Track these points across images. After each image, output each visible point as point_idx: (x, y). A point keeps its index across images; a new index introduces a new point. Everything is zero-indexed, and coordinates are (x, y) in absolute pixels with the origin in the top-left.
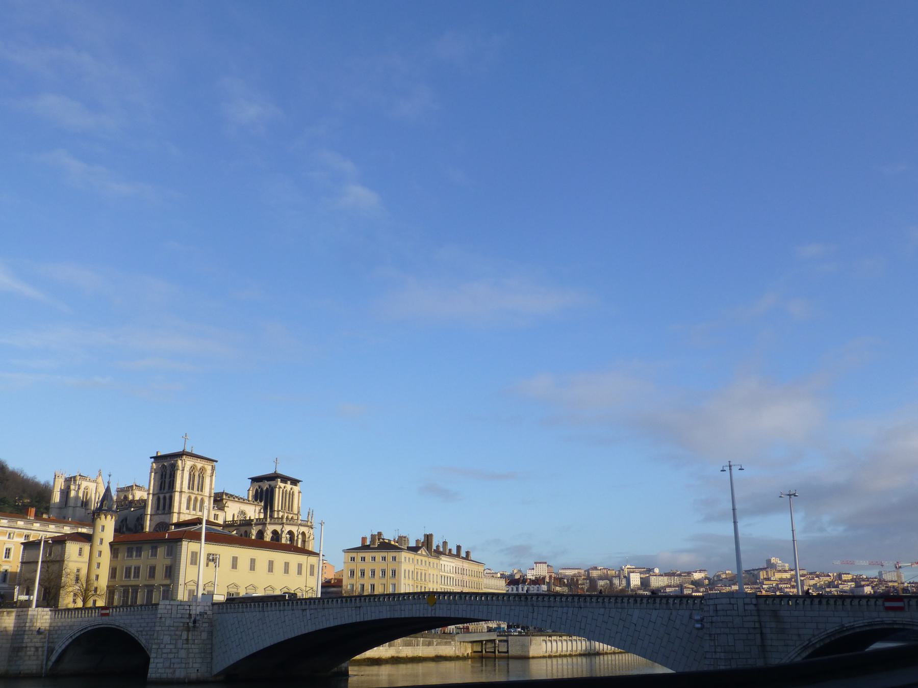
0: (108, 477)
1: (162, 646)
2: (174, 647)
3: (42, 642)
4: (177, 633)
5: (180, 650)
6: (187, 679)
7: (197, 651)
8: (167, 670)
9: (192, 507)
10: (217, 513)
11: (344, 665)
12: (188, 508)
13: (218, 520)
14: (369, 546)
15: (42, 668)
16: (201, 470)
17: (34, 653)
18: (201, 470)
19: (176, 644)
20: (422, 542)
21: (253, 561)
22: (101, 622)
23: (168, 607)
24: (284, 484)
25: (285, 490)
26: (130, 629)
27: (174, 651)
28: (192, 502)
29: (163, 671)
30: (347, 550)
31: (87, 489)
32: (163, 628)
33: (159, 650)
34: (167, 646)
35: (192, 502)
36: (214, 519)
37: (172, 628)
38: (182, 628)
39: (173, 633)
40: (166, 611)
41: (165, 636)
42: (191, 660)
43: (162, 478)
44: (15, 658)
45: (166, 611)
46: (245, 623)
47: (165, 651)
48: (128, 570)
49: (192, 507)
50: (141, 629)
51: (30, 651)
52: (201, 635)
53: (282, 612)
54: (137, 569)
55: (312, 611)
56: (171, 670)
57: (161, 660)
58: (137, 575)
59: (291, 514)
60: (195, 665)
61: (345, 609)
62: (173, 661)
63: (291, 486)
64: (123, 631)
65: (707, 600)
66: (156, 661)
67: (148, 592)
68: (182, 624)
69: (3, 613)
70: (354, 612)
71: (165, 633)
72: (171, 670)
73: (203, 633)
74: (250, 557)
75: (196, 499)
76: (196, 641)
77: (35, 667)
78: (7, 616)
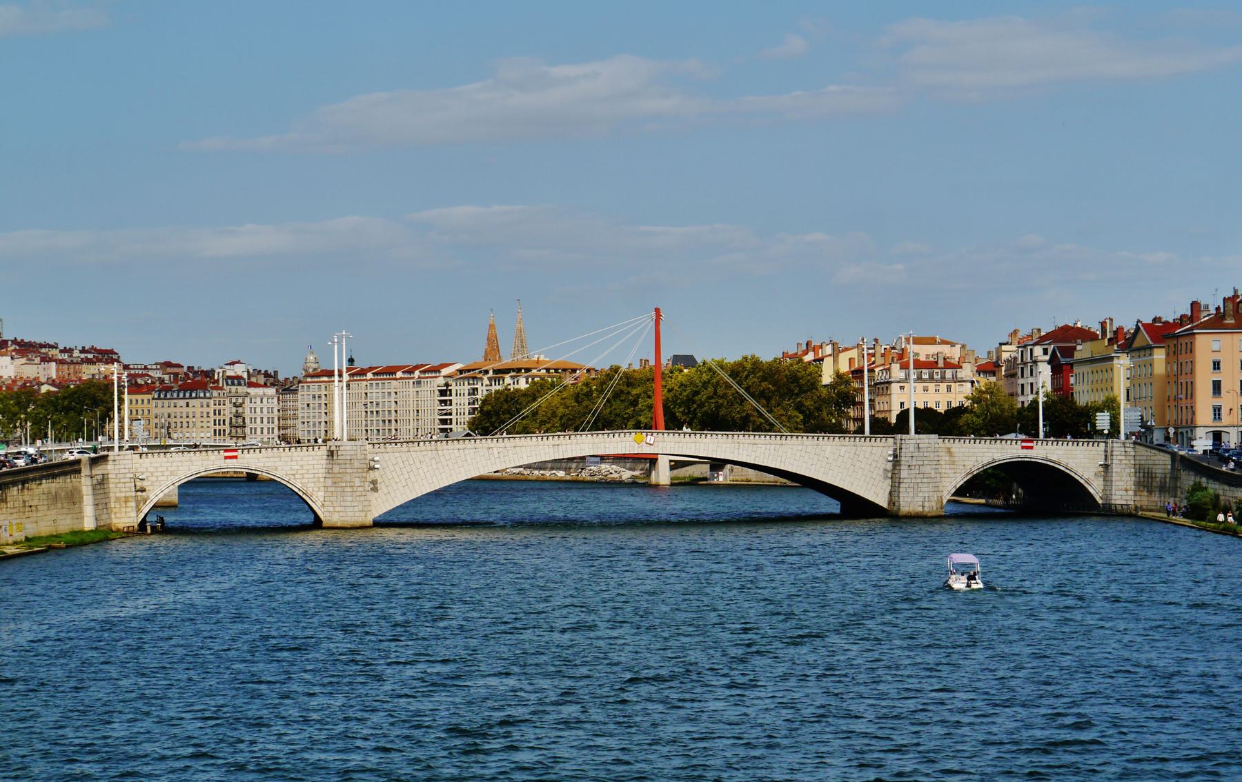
27: (363, 493)
37: (360, 470)
46: (411, 462)
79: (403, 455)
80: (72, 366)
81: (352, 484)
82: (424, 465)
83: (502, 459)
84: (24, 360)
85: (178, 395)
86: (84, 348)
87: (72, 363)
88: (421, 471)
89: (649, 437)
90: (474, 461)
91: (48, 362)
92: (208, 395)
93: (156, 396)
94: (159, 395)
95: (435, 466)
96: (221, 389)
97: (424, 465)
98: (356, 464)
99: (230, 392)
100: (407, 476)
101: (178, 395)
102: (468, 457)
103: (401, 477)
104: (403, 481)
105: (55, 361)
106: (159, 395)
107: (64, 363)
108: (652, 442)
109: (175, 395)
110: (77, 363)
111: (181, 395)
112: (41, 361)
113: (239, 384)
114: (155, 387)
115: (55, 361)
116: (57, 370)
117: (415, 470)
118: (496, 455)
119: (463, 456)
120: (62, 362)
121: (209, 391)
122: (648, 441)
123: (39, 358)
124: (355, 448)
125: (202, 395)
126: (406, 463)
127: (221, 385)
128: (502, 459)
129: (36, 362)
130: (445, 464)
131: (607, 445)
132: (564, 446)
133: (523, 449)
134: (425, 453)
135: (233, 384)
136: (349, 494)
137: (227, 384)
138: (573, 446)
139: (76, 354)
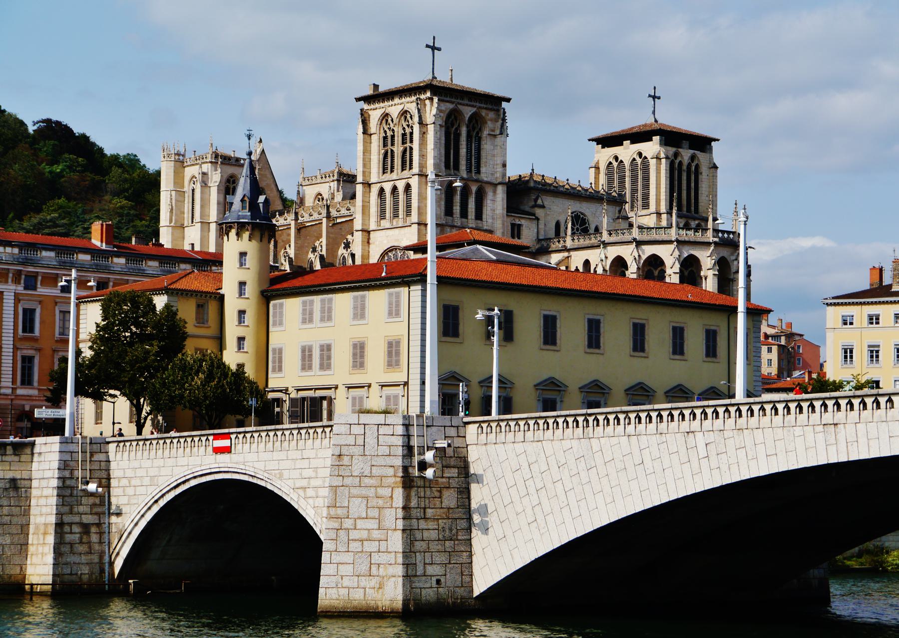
0: (246, 138)
1: (348, 524)
2: (376, 526)
3: (96, 514)
4: (381, 491)
5: (390, 532)
6: (412, 602)
7: (434, 535)
8: (364, 582)
9: (457, 209)
10: (518, 222)
11: (816, 573)
12: (408, 187)
14: (890, 286)
15: (102, 571)
16: (474, 121)
17: (81, 538)
18: (474, 121)
22: (214, 467)
24: (674, 149)
25: (677, 161)
26: (278, 483)
27: (376, 534)
28: (457, 198)
29: (353, 582)
30: (834, 298)
31: (234, 182)
32: (348, 481)
33: (342, 533)
34: (360, 524)
35: (457, 198)
36: (513, 237)
37: (367, 481)
38: (393, 479)
39: (371, 492)
40: (351, 440)
41: (352, 500)
42: (419, 557)
43: (385, 145)
44: (40, 549)
47: (354, 535)
48: (306, 354)
49: (457, 209)
50: (304, 483)
51: (71, 533)
52: (440, 497)
54: (326, 349)
55: (711, 437)
56: (374, 582)
57: (348, 558)
58: (326, 364)
59: (695, 219)
60: (430, 570)
61: (798, 431)
62: (376, 558)
63: (692, 151)
64: (265, 489)
66: (336, 558)
69: (5, 449)
70: (820, 437)
71: (354, 491)
72: (374, 582)
73: (446, 493)
74: (587, 317)
75: (465, 191)
76: (430, 513)
77: (86, 570)
78: (15, 455)
81: (340, 512)
117: (549, 485)
118: (702, 453)
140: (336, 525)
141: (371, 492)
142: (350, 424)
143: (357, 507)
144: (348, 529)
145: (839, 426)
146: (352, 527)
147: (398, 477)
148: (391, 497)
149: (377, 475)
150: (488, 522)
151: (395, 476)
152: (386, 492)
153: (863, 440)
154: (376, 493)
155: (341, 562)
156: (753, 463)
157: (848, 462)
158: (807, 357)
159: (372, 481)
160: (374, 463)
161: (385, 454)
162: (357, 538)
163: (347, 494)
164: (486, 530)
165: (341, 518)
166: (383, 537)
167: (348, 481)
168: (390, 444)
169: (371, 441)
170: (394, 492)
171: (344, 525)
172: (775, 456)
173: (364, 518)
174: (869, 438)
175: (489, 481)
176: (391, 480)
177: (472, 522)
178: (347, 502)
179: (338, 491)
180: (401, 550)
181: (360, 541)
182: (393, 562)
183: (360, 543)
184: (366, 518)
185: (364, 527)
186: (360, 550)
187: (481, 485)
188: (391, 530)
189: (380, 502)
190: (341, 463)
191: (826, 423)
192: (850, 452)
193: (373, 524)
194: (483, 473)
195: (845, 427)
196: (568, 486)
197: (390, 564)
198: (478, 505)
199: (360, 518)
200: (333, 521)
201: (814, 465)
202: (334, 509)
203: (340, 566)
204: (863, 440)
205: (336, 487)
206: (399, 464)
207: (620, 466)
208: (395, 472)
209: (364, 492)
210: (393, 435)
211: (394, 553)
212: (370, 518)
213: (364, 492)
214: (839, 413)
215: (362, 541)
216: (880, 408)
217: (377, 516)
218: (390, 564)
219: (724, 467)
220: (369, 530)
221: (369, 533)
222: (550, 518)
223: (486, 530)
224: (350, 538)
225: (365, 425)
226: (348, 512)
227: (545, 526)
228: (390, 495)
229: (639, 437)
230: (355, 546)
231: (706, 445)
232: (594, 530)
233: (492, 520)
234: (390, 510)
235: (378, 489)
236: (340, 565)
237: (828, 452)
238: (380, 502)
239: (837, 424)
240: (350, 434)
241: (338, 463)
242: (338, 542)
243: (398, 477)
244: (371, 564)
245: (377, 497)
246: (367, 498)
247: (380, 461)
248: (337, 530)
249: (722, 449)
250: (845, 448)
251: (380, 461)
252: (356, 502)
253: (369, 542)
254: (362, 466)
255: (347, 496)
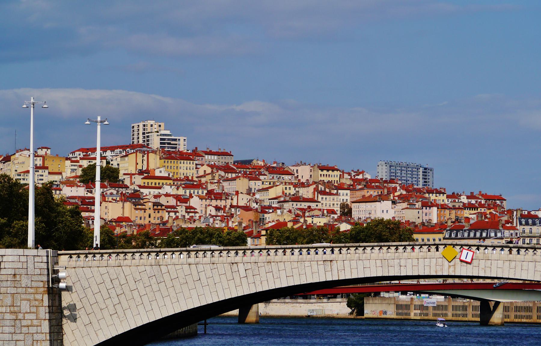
1: (20, 316)
2: (35, 318)
5: (42, 321)
13: (207, 167)
19: (37, 313)
20: (407, 192)
21: (419, 212)
23: (23, 259)
27: (35, 322)
32: (20, 290)
33: (17, 322)
34: (27, 316)
37: (30, 290)
39: (31, 297)
40: (20, 265)
45: (20, 264)
46: (123, 281)
47: (24, 323)
53: (193, 267)
55: (248, 266)
62: (36, 337)
65: (514, 270)
67: (458, 235)
68: (41, 284)
70: (321, 267)
71: (23, 296)
79: (111, 270)
80: (453, 212)
81: (16, 309)
82: (140, 286)
83: (251, 279)
84: (405, 205)
85: (469, 235)
86: (472, 193)
87: (454, 208)
88: (135, 293)
89: (465, 252)
90: (210, 281)
91: (430, 207)
92: (499, 235)
93: (447, 236)
94: (450, 235)
95: (155, 287)
96: (514, 228)
97: (140, 286)
98: (25, 281)
99: (524, 232)
100: (116, 301)
101: (469, 235)
102: (202, 275)
103: (108, 302)
104: (111, 307)
105: (437, 206)
106: (450, 235)
107: (446, 208)
108: (469, 260)
109: (466, 235)
110: (459, 208)
111: (472, 235)
112: (423, 206)
113: (534, 224)
114: (446, 227)
115: (437, 206)
116: (439, 216)
117: (127, 292)
118: (243, 274)
119: (195, 273)
120: (443, 207)
121: (500, 231)
122: (463, 258)
123: (420, 203)
124: (23, 259)
125: (493, 234)
126: (116, 282)
127: (515, 225)
128: (251, 279)
129: (417, 206)
130: (169, 284)
131: (403, 262)
132: (340, 263)
133: (281, 265)
134: (142, 268)
135: (527, 224)
136: (8, 323)
137: (521, 224)
138: (354, 263)
139: (464, 199)
140: (14, 317)
141: (31, 297)
142: (19, 256)
143: (25, 306)
144: (21, 320)
145: (333, 262)
146: (22, 318)
147: (45, 287)
148: (42, 300)
149: (35, 286)
150: (76, 315)
151: (44, 287)
152: (39, 297)
153: (347, 269)
154: (34, 297)
155: (18, 339)
156: (277, 281)
157: (377, 277)
158: (411, 227)
159: (32, 290)
160: (33, 279)
161: (38, 274)
162: (25, 324)
163: (19, 298)
164: (74, 319)
165: (17, 313)
166: (39, 324)
167: (20, 290)
168: (40, 268)
169: (31, 265)
170: (44, 297)
171: (18, 317)
172: (292, 277)
173: (28, 313)
174: (351, 268)
175: (77, 290)
176: (42, 290)
177: (63, 315)
178: (19, 303)
179: (14, 297)
180: (48, 332)
181: (27, 326)
182: (45, 339)
183: (27, 328)
184: (30, 313)
185: (29, 318)
186: (27, 332)
187: (70, 292)
188: (43, 320)
189: (37, 303)
190: (15, 279)
191: (325, 260)
192: (340, 275)
193: (33, 316)
194: (72, 285)
195: (337, 263)
196: (143, 292)
197: (43, 340)
198: (68, 304)
199: (27, 313)
200: (13, 315)
201: (317, 282)
202: (13, 307)
203: (17, 342)
204: (347, 269)
205: (13, 294)
206: (45, 280)
207: (183, 281)
208: (44, 285)
209: (28, 297)
210: (42, 262)
211: (45, 334)
212: (32, 313)
213: (28, 297)
214: (333, 255)
215: (28, 326)
216: (511, 254)
217: (35, 311)
218: (43, 340)
219: (258, 283)
220: (31, 320)
221: (31, 321)
222: (128, 312)
223: (74, 319)
224: (22, 325)
225: (27, 256)
226: (20, 309)
227: (124, 316)
228: (41, 299)
229: (197, 265)
230: (24, 330)
231: (246, 270)
232: (163, 318)
233: (80, 314)
234: (42, 307)
235: (35, 295)
236: (17, 341)
237: (326, 275)
238: (37, 303)
239: (332, 261)
240: (19, 262)
241: (14, 279)
242: (16, 328)
243: (45, 287)
244: (33, 340)
245: (35, 300)
246: (29, 300)
247: (35, 278)
248: (15, 320)
249: (256, 272)
250: (337, 273)
251: (35, 278)
252: (24, 303)
253: (32, 327)
254: (26, 281)
255: (20, 300)
